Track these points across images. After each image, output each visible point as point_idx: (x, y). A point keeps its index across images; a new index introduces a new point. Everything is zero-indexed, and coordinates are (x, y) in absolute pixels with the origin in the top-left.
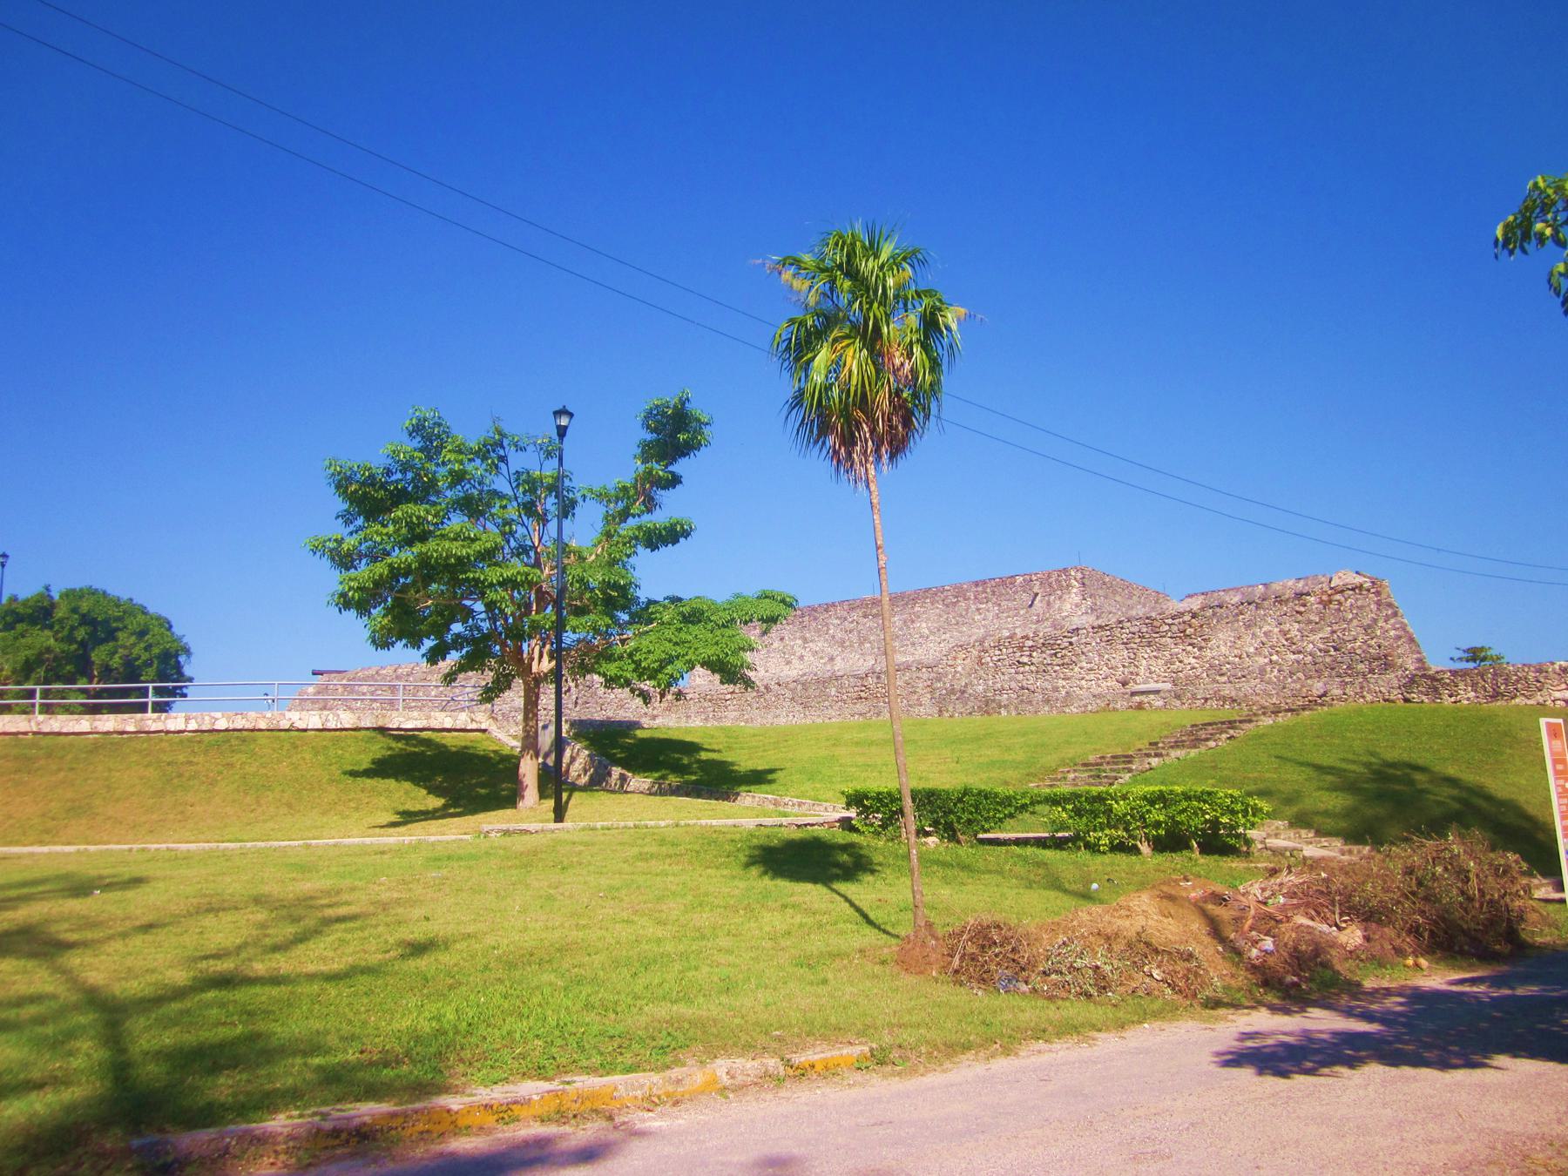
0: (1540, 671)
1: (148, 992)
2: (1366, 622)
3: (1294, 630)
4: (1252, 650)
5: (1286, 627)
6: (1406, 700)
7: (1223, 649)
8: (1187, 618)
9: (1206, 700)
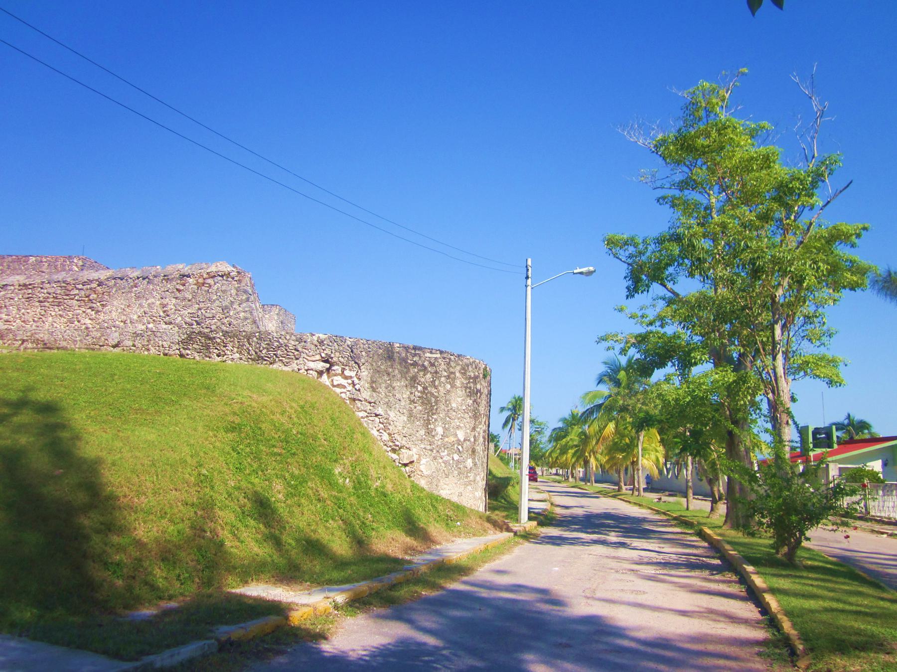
0: (300, 340)
1: (743, 626)
2: (225, 303)
3: (171, 303)
4: (135, 317)
5: (165, 301)
6: (182, 356)
7: (114, 314)
8: (94, 285)
9: (23, 341)
